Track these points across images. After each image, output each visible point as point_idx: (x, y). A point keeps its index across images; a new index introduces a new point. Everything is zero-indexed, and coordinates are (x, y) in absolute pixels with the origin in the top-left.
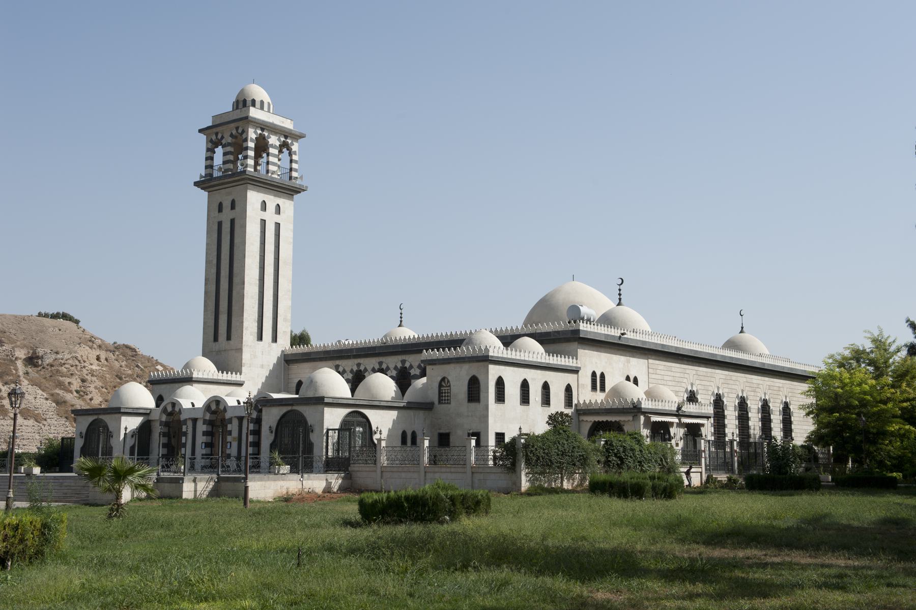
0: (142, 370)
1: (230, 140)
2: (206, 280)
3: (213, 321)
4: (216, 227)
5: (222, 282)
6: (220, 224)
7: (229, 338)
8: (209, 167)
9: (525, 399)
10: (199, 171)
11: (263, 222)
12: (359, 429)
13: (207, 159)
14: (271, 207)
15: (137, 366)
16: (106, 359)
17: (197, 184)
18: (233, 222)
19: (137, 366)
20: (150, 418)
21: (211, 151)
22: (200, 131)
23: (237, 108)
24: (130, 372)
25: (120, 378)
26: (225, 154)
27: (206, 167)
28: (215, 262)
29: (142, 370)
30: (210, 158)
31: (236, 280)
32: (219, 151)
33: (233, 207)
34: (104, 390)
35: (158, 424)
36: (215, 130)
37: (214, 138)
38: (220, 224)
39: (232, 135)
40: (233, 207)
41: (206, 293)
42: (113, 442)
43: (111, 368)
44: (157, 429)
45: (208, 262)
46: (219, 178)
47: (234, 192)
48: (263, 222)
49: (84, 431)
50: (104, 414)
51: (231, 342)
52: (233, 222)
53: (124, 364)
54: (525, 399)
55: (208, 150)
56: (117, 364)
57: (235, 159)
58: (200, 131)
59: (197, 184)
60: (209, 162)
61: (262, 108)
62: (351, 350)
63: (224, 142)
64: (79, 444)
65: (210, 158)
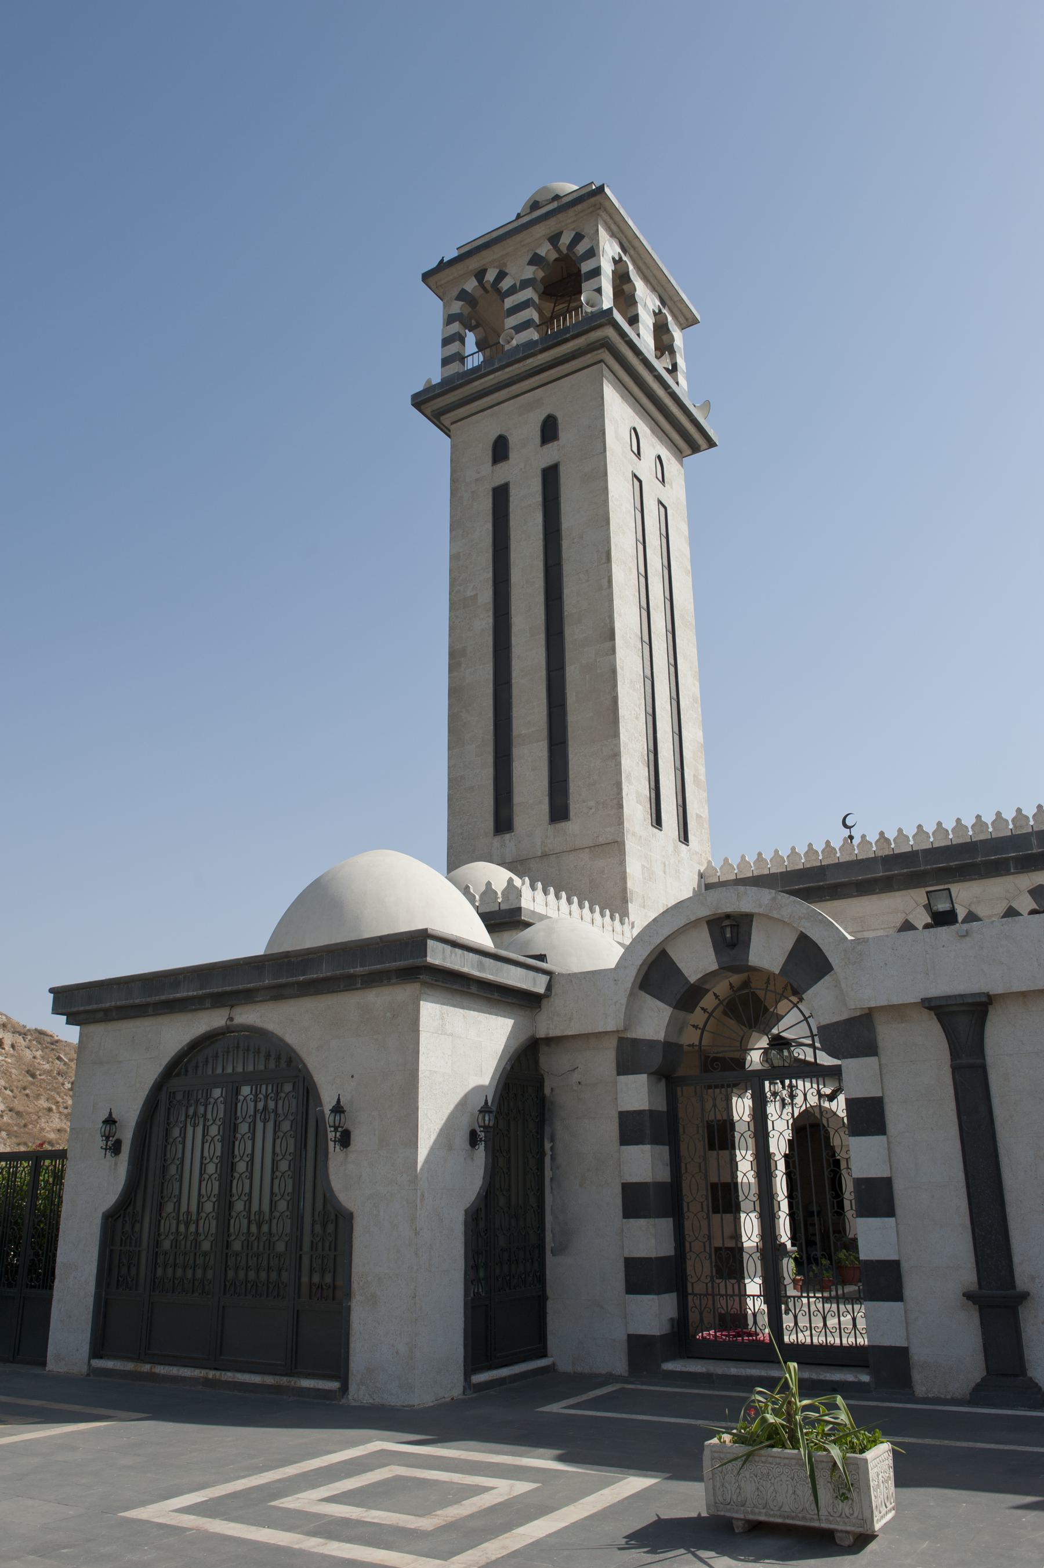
0: (65, 1064)
2: (453, 654)
3: (490, 771)
4: (486, 504)
6: (501, 495)
7: (559, 812)
13: (446, 342)
15: (59, 1058)
16: (13, 1046)
18: (551, 476)
19: (59, 1058)
20: (547, 1026)
24: (47, 1067)
25: (33, 1076)
28: (486, 596)
29: (65, 1064)
31: (573, 633)
34: (8, 1092)
35: (603, 1061)
36: (474, 264)
38: (501, 495)
41: (455, 692)
42: (353, 1178)
43: (19, 1059)
44: (606, 1097)
47: (553, 398)
49: (130, 1114)
50: (278, 993)
51: (572, 827)
52: (551, 476)
53: (39, 1054)
56: (28, 1054)
57: (537, 322)
62: (1016, 841)
64: (92, 1190)
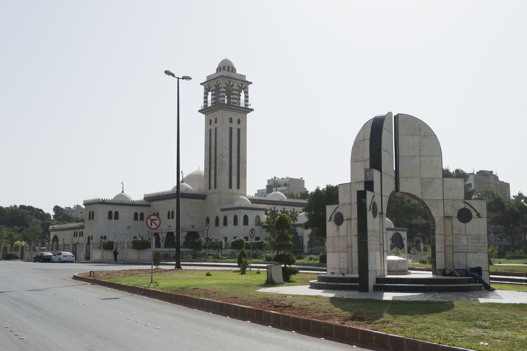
1: (214, 88)
5: (233, 159)
6: (210, 130)
8: (206, 102)
9: (236, 223)
10: (201, 105)
11: (231, 129)
12: (523, 201)
14: (235, 120)
17: (200, 111)
18: (239, 130)
21: (206, 94)
22: (201, 84)
23: (220, 70)
26: (212, 95)
27: (204, 102)
30: (246, 97)
32: (210, 93)
33: (211, 121)
37: (207, 87)
38: (210, 130)
39: (238, 86)
40: (211, 121)
45: (206, 151)
46: (242, 107)
48: (231, 129)
51: (240, 190)
52: (239, 130)
54: (236, 223)
55: (205, 93)
58: (201, 84)
59: (200, 111)
60: (247, 99)
61: (228, 70)
63: (211, 89)
65: (206, 98)
